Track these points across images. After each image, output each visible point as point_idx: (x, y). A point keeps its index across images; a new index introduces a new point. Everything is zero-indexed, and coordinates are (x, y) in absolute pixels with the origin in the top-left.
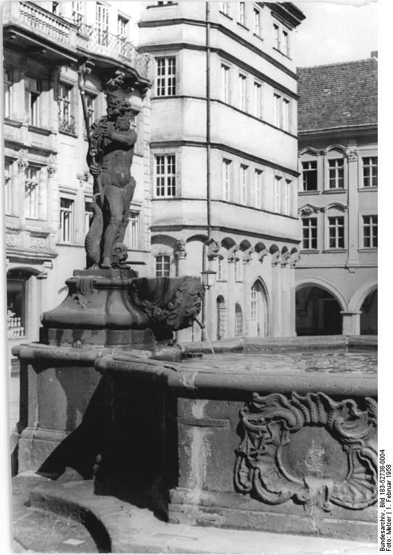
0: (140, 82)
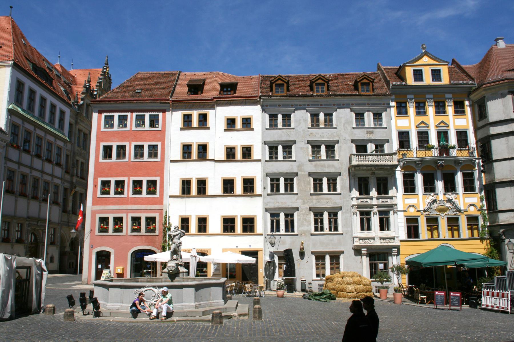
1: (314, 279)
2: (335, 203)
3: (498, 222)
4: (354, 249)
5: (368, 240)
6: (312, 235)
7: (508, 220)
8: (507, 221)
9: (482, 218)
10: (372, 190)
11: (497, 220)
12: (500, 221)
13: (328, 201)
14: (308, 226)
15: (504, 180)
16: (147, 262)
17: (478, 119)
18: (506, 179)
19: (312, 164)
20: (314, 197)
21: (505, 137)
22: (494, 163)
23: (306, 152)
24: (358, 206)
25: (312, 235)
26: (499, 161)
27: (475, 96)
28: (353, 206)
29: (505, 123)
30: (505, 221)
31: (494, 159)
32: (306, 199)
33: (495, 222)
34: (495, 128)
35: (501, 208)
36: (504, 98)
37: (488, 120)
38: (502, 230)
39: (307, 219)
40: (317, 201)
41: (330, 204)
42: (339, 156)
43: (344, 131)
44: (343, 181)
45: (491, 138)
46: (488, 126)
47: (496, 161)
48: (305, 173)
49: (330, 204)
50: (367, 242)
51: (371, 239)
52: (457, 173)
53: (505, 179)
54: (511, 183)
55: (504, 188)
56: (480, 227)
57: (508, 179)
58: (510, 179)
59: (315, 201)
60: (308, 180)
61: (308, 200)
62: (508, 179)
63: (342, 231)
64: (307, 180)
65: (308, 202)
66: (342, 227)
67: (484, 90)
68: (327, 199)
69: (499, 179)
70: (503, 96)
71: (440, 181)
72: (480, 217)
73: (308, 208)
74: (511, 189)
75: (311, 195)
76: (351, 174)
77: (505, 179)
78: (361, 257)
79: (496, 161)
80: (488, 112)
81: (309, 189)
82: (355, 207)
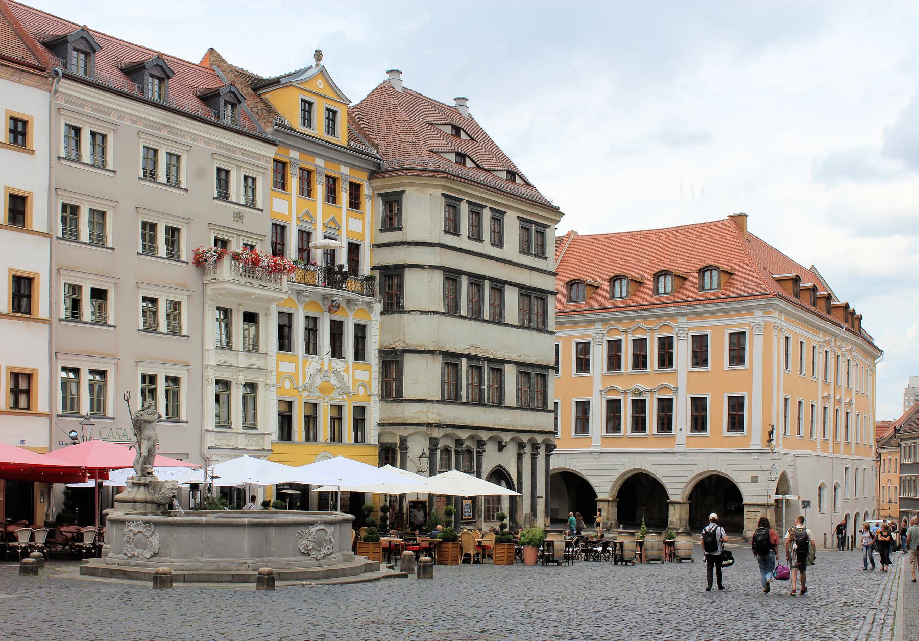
7: (417, 416)
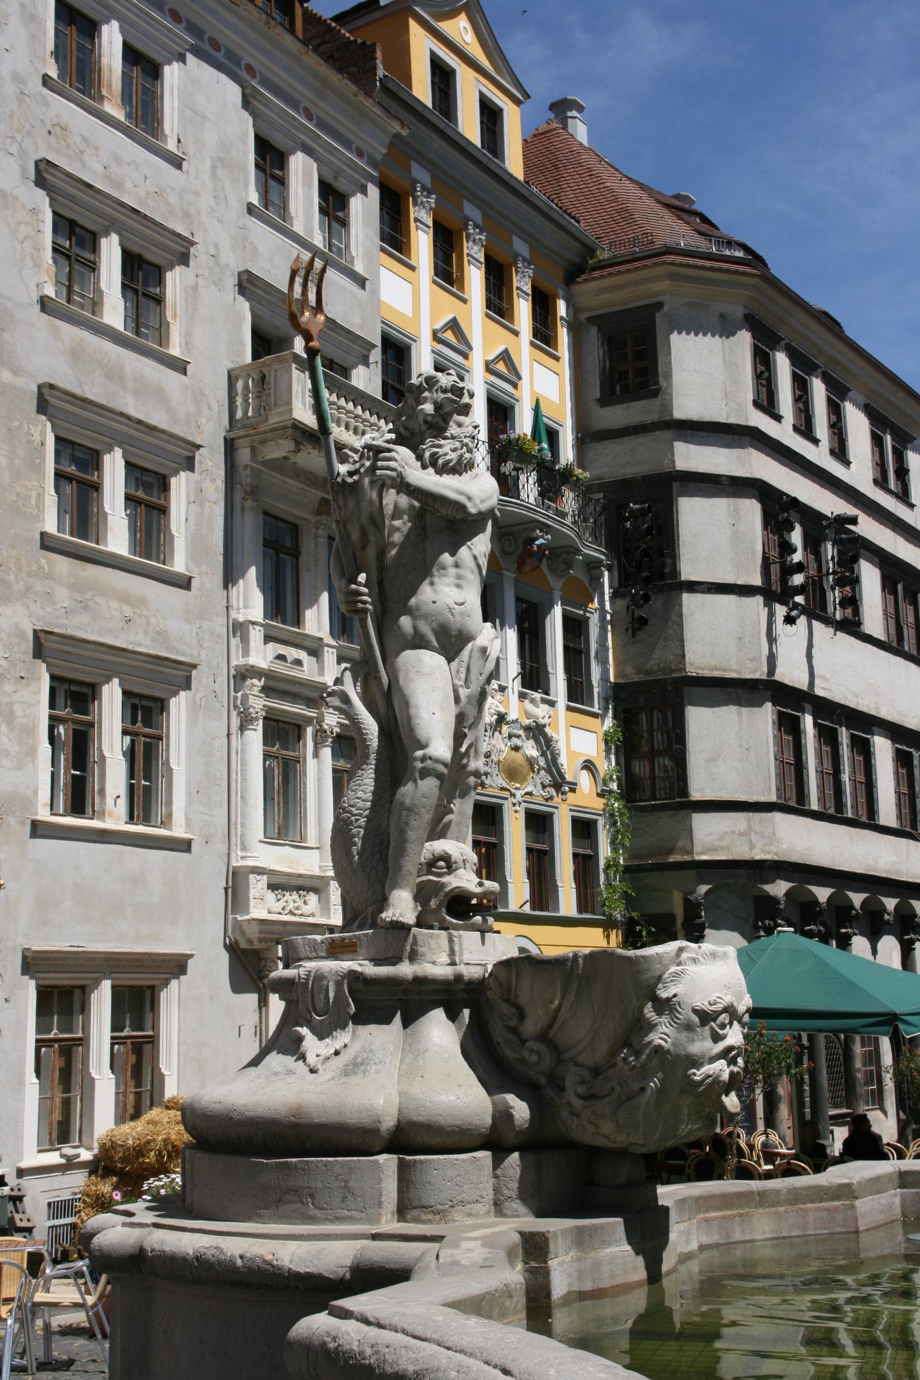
0: (585, 555)
1: (25, 1164)
2: (161, 635)
3: (690, 852)
4: (232, 948)
5: (295, 896)
6: (38, 830)
7: (725, 843)
8: (722, 848)
9: (609, 831)
10: (314, 600)
11: (681, 843)
12: (697, 847)
13: (128, 611)
14: (19, 767)
15: (716, 674)
16: (100, 1275)
17: (595, 392)
18: (725, 671)
19: (56, 331)
20: (63, 564)
21: (728, 495)
22: (685, 596)
23: (27, 237)
24: (272, 684)
25: (38, 830)
26: (703, 592)
27: (602, 291)
28: (243, 675)
29: (729, 437)
30: (714, 849)
31: (683, 578)
32: (20, 570)
33: (670, 852)
34: (692, 447)
35: (702, 790)
36: (727, 337)
37: (667, 407)
38: (703, 889)
39: (18, 710)
40: (78, 597)
41: (141, 637)
42: (187, 345)
43: (212, 202)
44: (202, 505)
45: (676, 486)
46: (667, 434)
47: (694, 587)
48: (20, 382)
49: (141, 637)
50: (291, 906)
51: (309, 889)
52: (553, 607)
53: (720, 669)
54: (740, 691)
55: (716, 709)
56: (601, 871)
57: (731, 670)
58: (738, 672)
59: (63, 595)
60: (37, 438)
61: (29, 575)
62: (731, 670)
63: (188, 823)
64: (29, 434)
65: (28, 589)
66: (190, 802)
67: (672, 277)
68: (126, 598)
69: (699, 668)
70: (726, 329)
71: (510, 628)
72: (601, 822)
73: (20, 634)
74: (739, 715)
75: (47, 543)
76: (245, 477)
77: (720, 669)
78: (254, 997)
79: (694, 587)
80: (669, 375)
81: (33, 501)
82: (255, 681)
